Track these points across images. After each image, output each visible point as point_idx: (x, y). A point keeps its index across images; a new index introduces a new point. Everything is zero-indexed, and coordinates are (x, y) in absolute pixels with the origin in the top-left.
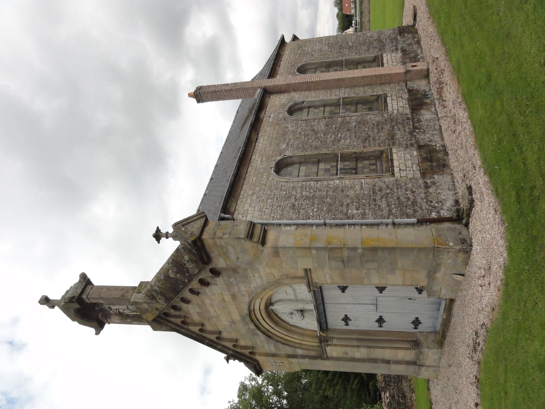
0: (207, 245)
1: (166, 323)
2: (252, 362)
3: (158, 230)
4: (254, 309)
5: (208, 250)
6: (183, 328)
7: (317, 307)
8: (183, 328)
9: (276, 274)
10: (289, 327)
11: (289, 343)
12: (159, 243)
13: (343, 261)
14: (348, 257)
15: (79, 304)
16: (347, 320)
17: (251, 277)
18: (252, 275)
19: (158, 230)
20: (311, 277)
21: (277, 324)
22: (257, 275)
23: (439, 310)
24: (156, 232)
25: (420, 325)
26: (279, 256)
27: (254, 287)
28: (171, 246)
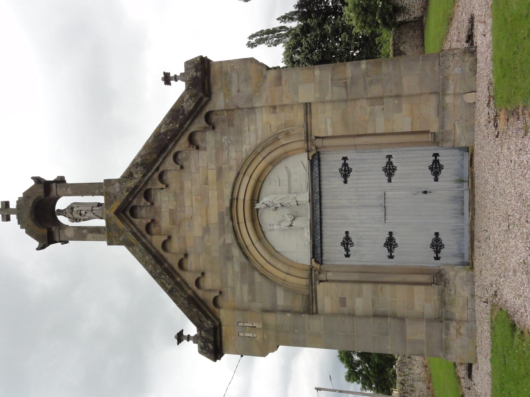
0: (212, 73)
1: (129, 223)
2: (213, 318)
3: (181, 332)
4: (237, 199)
5: (212, 81)
6: (145, 237)
7: (312, 200)
8: (145, 237)
9: (273, 123)
10: (273, 252)
11: (269, 276)
12: (178, 344)
13: (346, 86)
14: (352, 77)
15: (57, 218)
16: (347, 244)
17: (245, 132)
18: (247, 129)
19: (181, 332)
20: (311, 123)
21: (260, 239)
22: (252, 128)
23: (463, 214)
24: (180, 332)
25: (442, 250)
26: (280, 84)
27: (246, 150)
28: (179, 88)
